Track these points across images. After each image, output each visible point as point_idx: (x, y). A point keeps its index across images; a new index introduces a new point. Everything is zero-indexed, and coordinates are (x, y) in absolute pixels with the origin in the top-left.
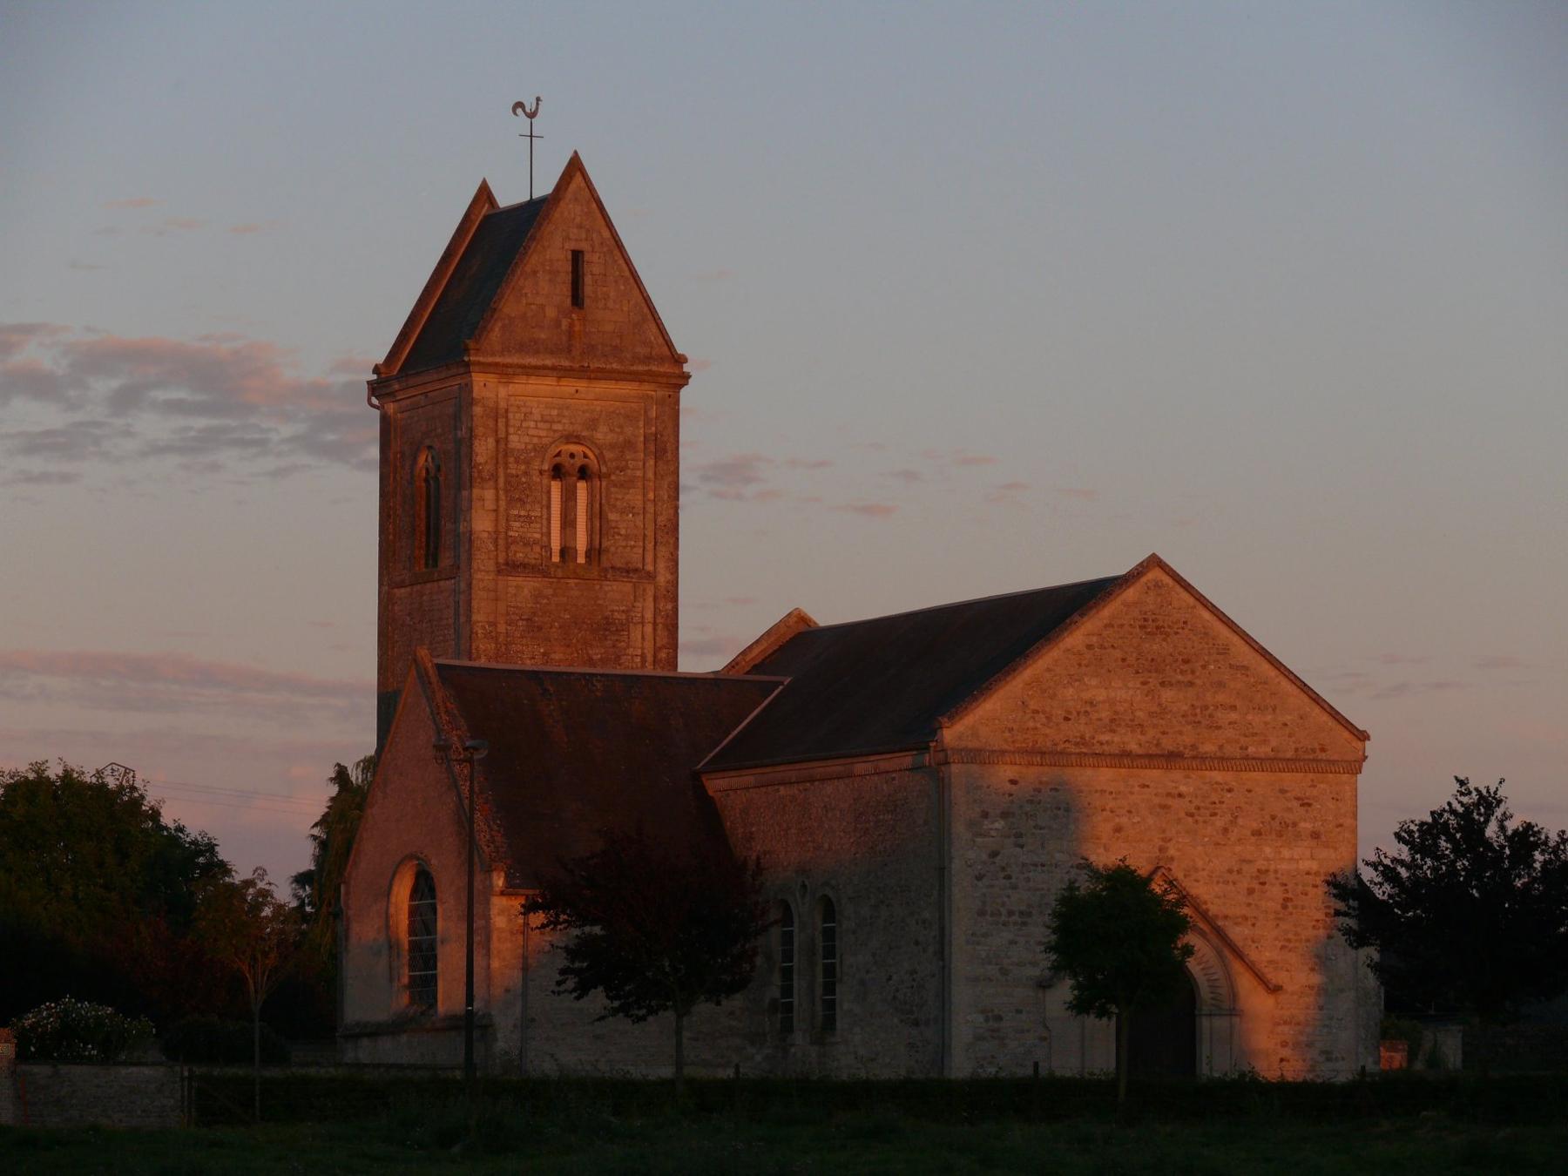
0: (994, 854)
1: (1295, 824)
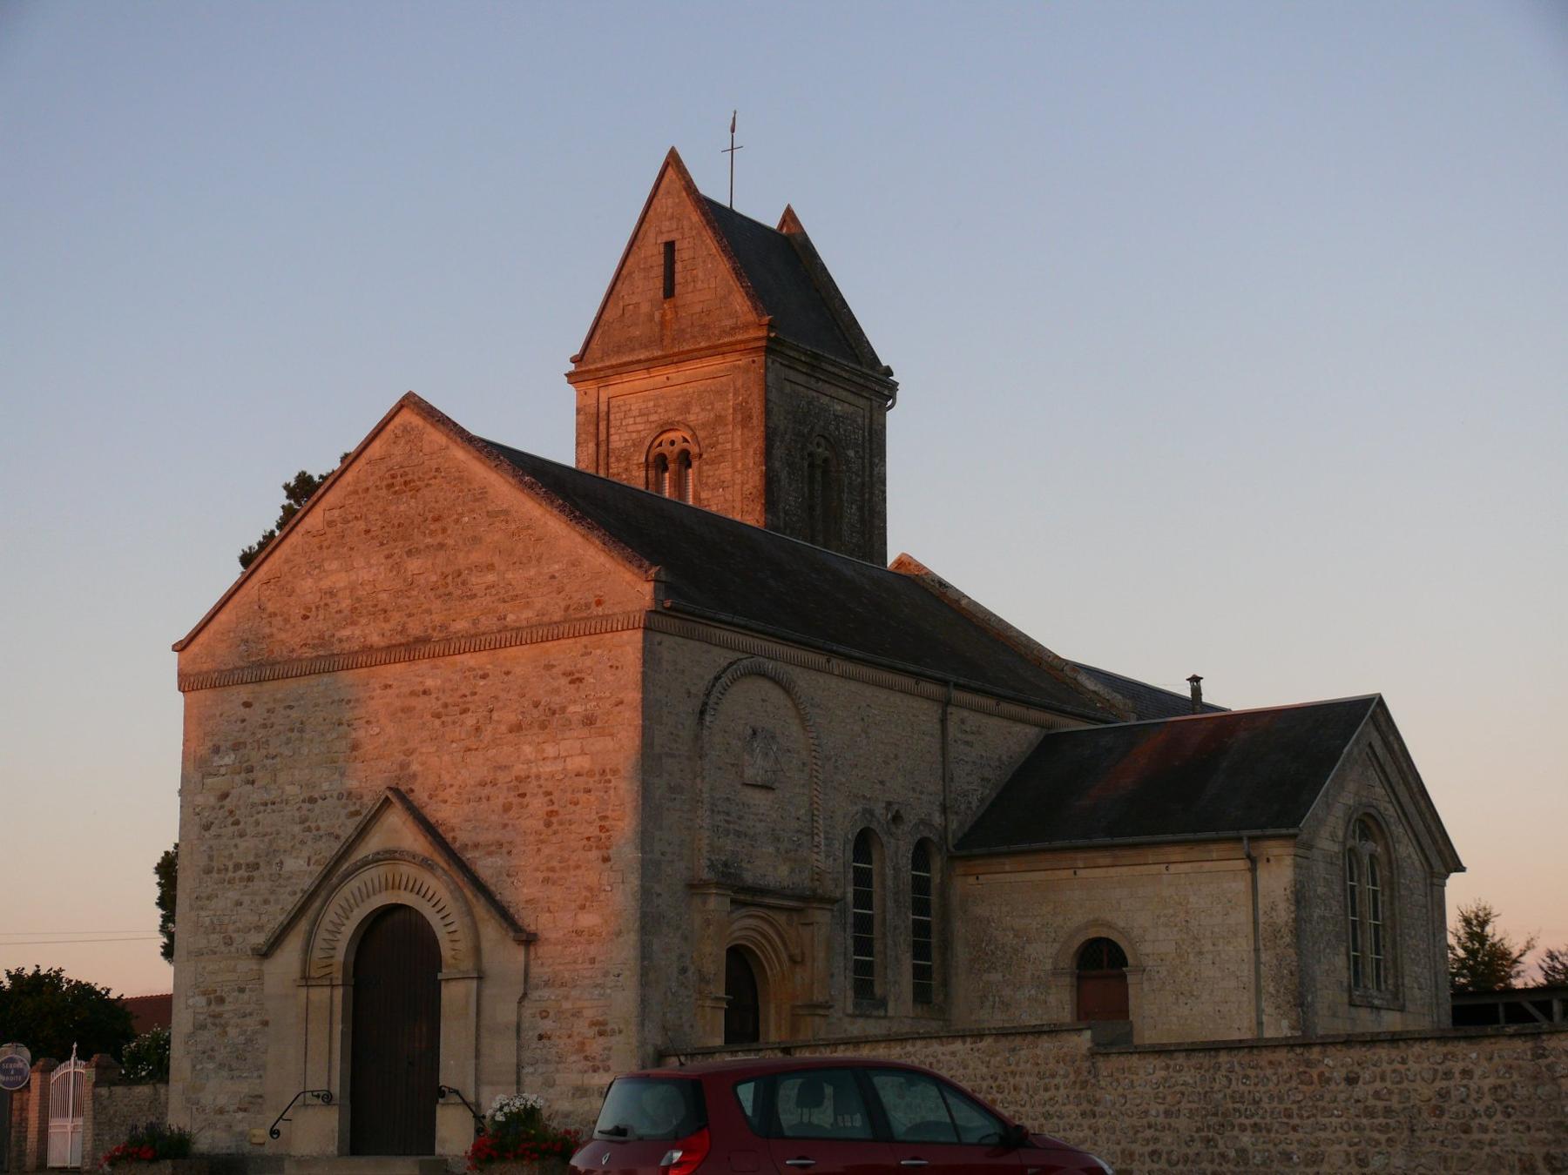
0: (225, 796)
1: (563, 709)
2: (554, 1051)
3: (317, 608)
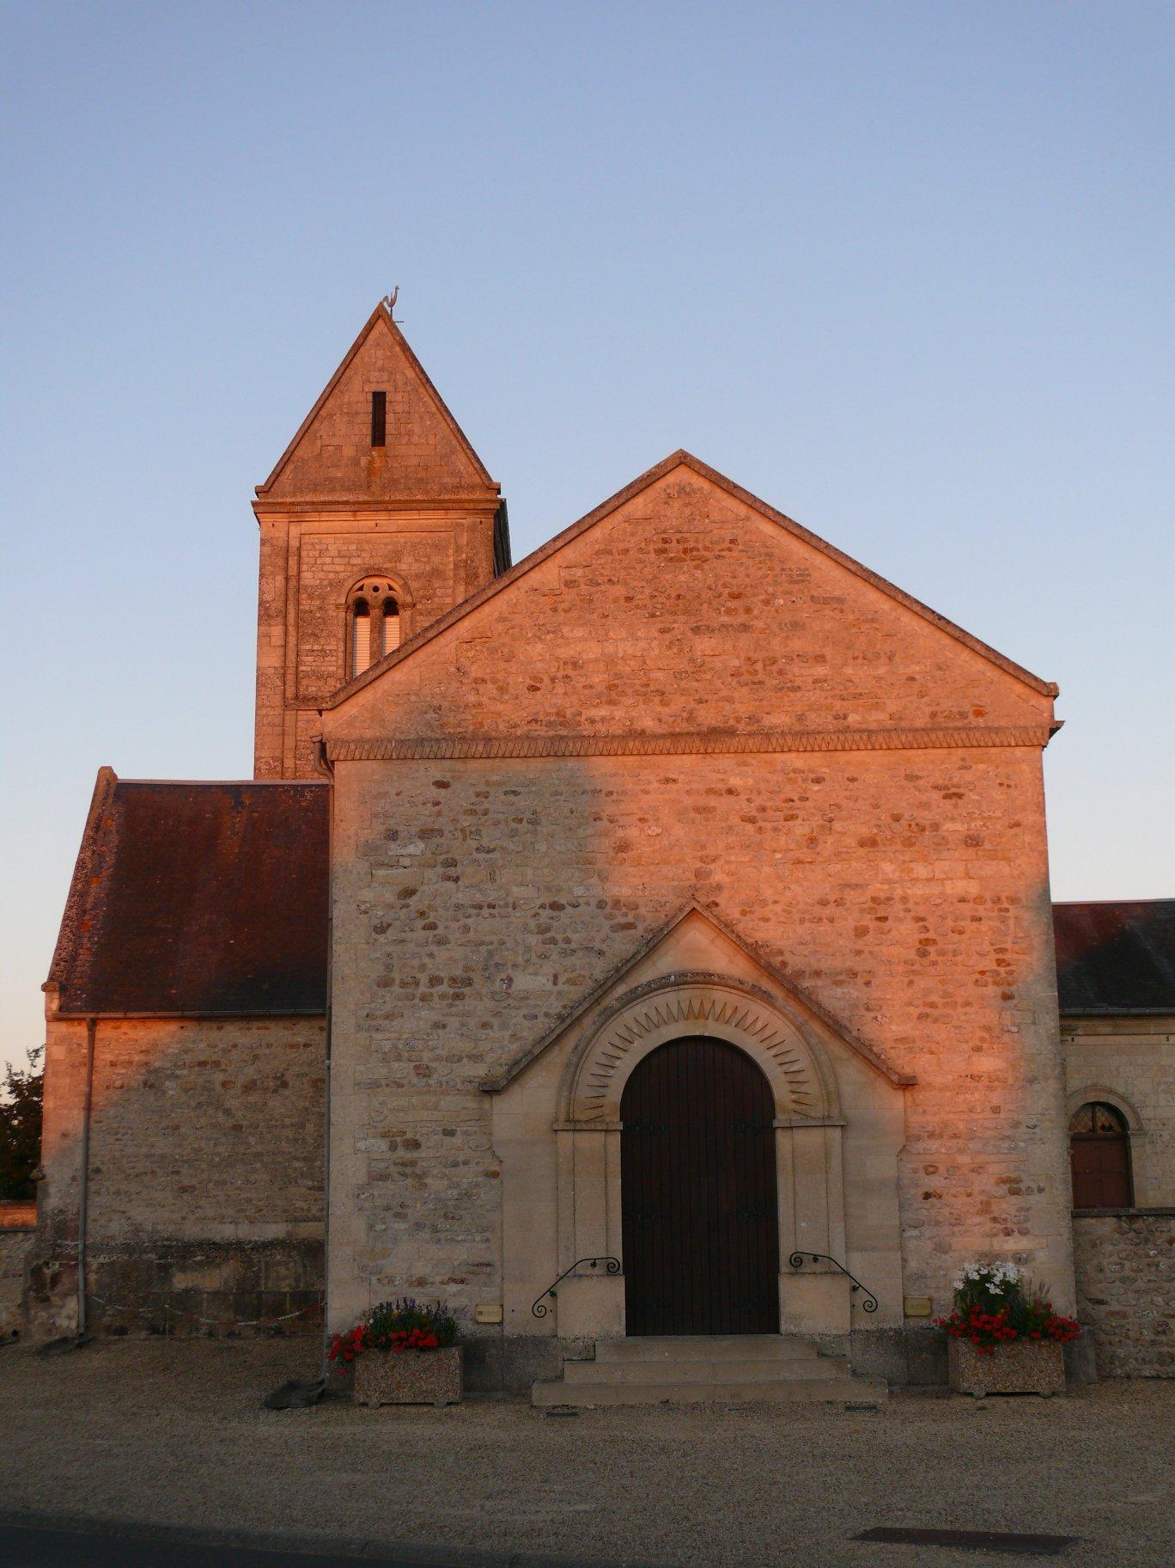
0: (409, 893)
1: (936, 827)
2: (946, 1211)
3: (553, 680)
